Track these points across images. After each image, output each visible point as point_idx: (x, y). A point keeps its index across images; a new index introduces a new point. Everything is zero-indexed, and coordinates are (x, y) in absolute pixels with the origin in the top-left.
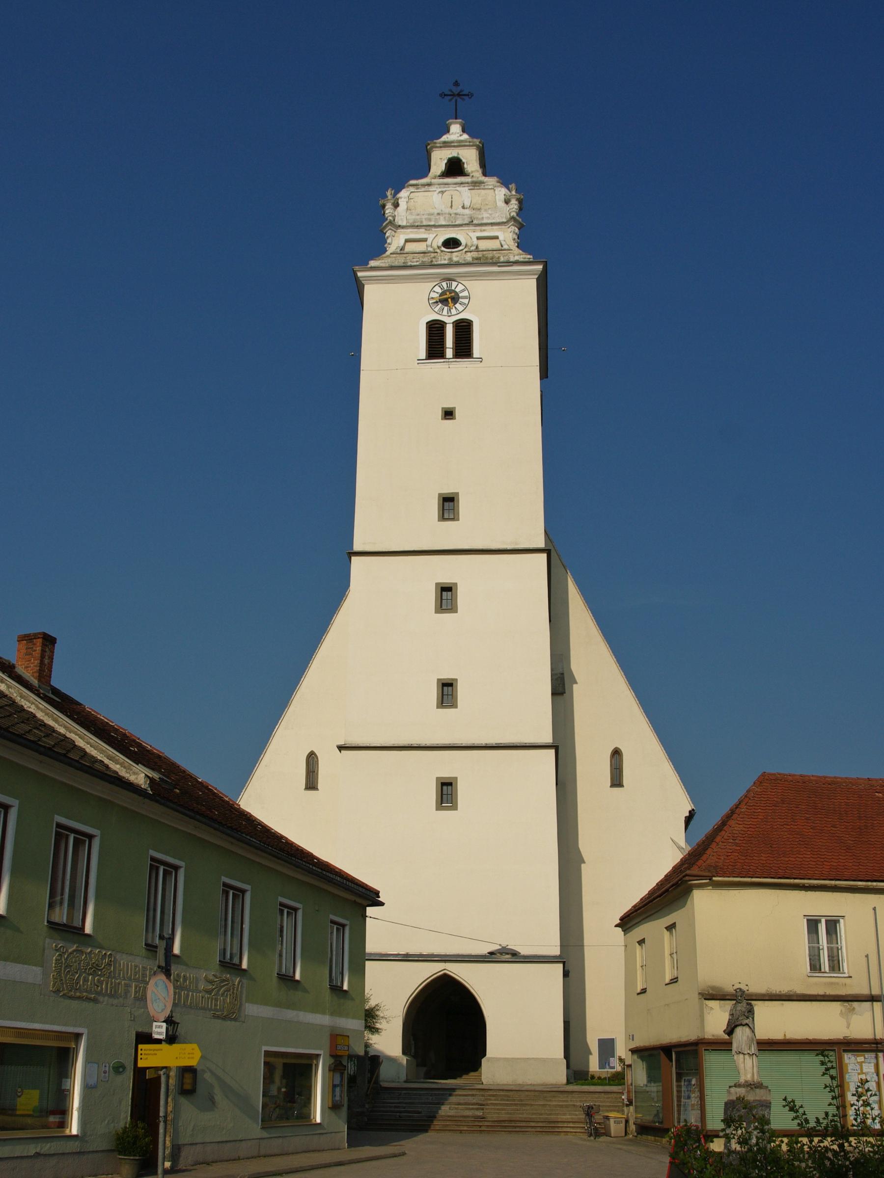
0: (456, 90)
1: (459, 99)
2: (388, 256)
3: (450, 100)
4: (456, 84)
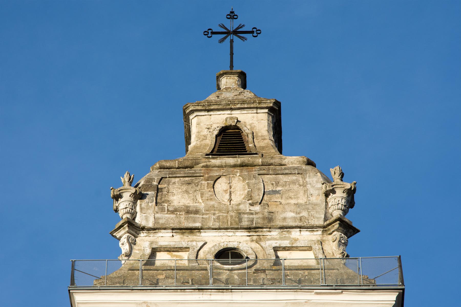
0: (231, 25)
1: (235, 38)
2: (202, 241)
3: (222, 41)
4: (232, 16)
